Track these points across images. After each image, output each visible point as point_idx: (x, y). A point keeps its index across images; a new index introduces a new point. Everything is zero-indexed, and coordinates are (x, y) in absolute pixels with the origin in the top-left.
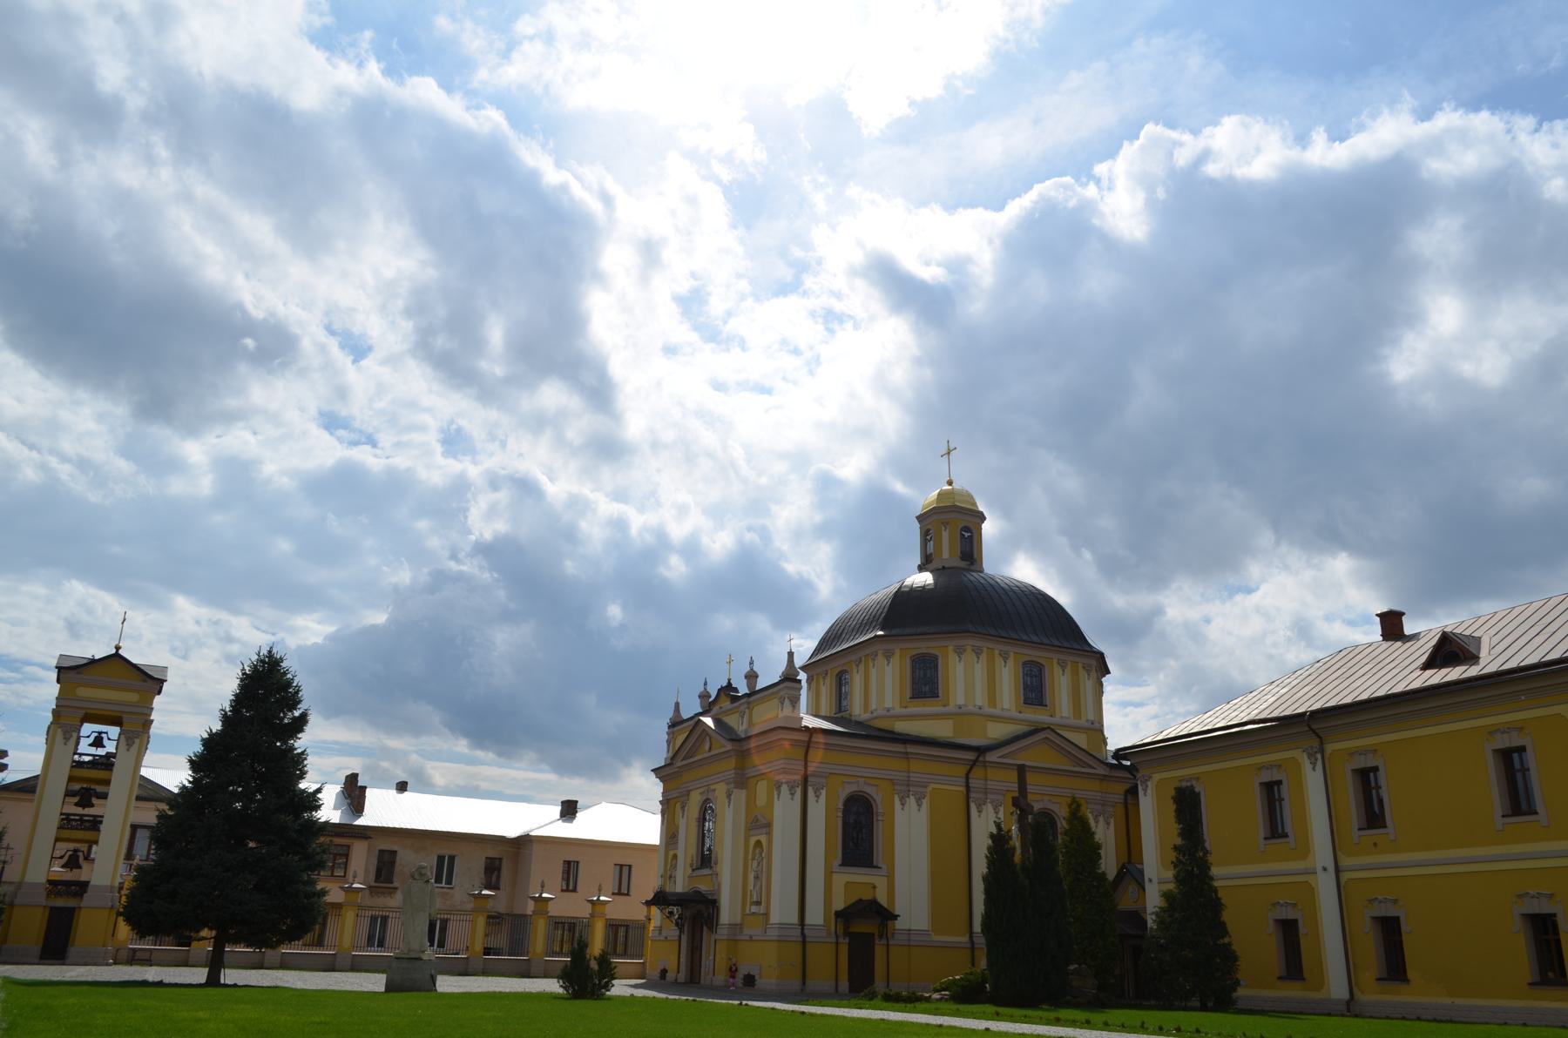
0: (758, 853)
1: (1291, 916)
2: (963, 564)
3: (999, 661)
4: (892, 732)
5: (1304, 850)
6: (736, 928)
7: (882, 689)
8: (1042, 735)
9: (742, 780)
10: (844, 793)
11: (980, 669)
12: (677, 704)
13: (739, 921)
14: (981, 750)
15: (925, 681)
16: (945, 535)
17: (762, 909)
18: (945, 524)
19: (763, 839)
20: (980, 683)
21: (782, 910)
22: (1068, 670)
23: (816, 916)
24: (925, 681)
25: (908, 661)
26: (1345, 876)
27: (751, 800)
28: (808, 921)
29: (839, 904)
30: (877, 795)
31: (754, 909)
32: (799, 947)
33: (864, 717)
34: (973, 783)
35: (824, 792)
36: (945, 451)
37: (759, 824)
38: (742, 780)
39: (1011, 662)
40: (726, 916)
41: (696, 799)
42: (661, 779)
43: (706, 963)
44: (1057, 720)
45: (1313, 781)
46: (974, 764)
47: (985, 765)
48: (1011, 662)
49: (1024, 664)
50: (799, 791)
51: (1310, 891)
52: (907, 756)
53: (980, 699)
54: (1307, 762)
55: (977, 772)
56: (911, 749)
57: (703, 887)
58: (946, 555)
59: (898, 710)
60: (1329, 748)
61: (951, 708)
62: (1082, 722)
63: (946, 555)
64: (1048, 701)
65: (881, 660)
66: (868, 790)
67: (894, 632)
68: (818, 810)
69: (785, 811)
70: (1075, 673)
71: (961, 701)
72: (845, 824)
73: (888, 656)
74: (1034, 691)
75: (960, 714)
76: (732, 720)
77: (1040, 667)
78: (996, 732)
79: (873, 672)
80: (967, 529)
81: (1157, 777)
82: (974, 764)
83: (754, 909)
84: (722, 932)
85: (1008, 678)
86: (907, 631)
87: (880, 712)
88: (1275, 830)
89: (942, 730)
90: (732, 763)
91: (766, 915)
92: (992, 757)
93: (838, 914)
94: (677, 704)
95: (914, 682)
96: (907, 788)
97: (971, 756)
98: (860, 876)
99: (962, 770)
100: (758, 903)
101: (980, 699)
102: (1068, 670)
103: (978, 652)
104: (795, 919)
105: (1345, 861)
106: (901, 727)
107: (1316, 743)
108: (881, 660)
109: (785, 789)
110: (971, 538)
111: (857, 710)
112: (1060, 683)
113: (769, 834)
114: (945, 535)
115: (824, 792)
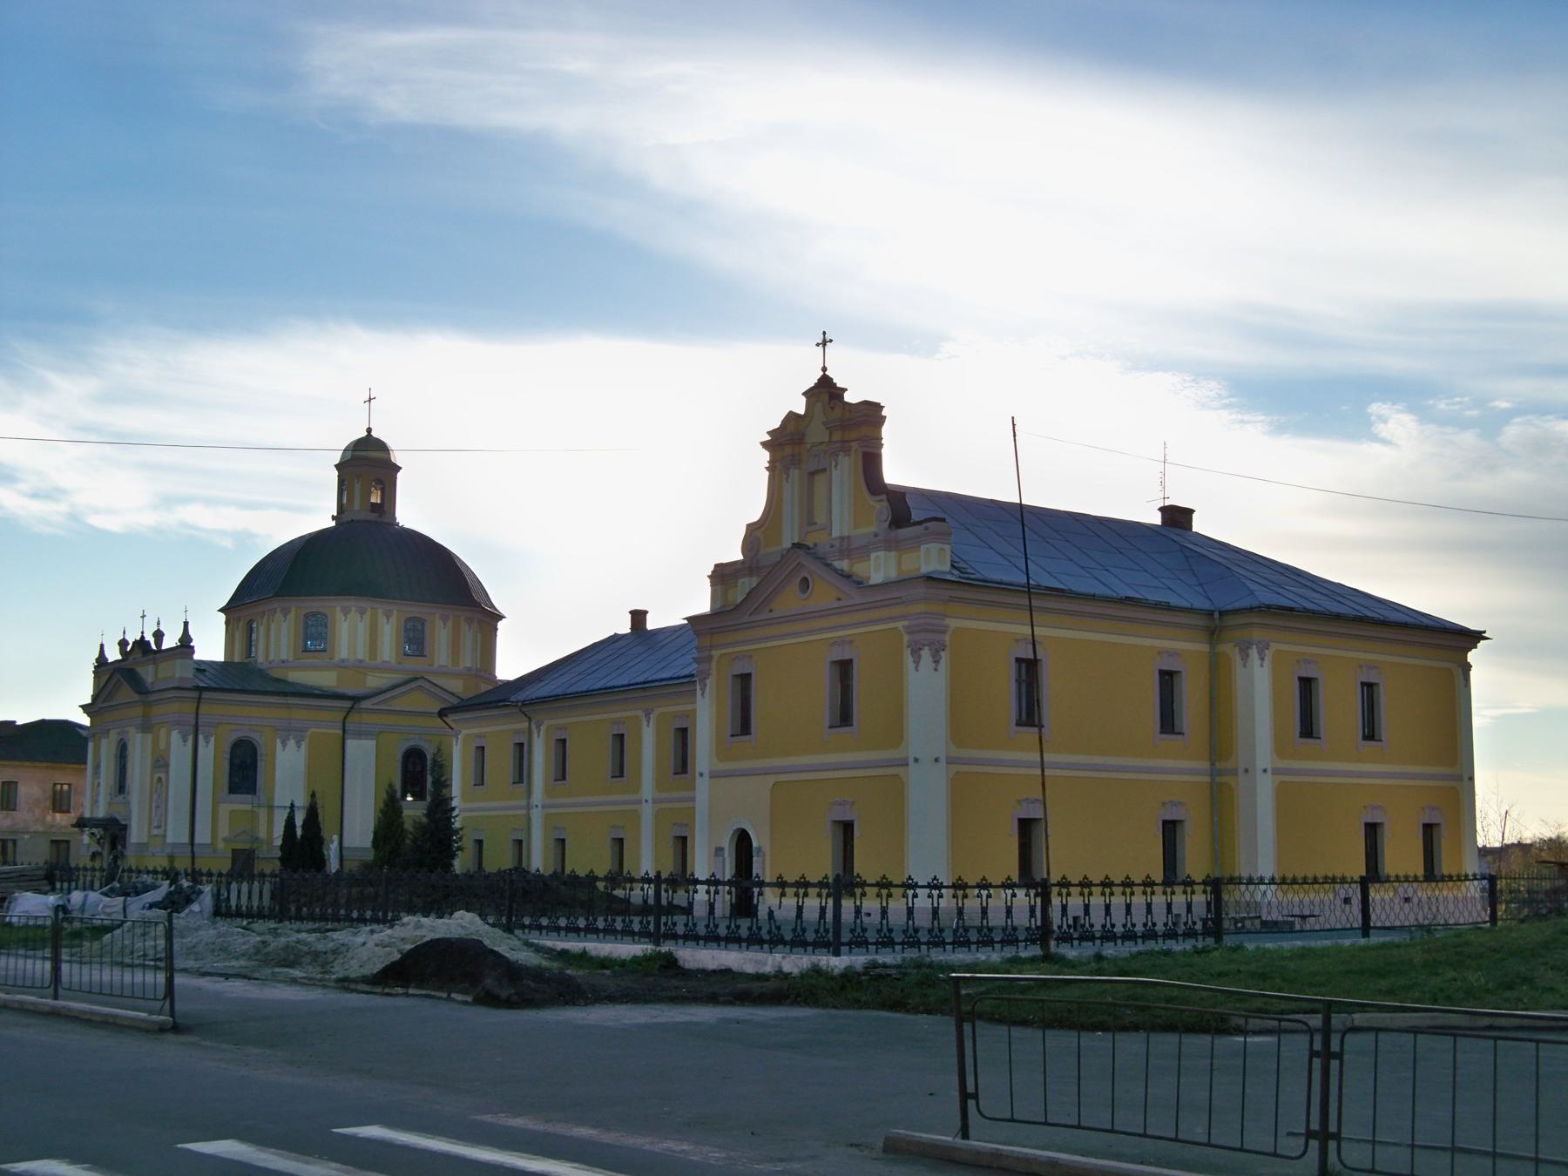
3: (382, 619)
4: (284, 681)
5: (637, 787)
8: (419, 683)
9: (146, 727)
10: (233, 737)
11: (362, 628)
12: (102, 646)
13: (145, 840)
14: (356, 699)
15: (315, 634)
19: (163, 776)
20: (362, 635)
21: (176, 833)
22: (450, 623)
27: (155, 742)
28: (197, 840)
30: (260, 739)
35: (213, 739)
37: (161, 763)
39: (393, 619)
46: (350, 710)
47: (360, 711)
48: (393, 619)
49: (408, 620)
52: (288, 706)
53: (362, 653)
54: (1238, 658)
56: (291, 700)
65: (279, 615)
66: (252, 735)
68: (207, 753)
72: (231, 760)
74: (415, 639)
75: (342, 666)
77: (423, 622)
78: (374, 681)
79: (273, 626)
81: (658, 711)
82: (350, 710)
83: (156, 832)
85: (389, 632)
88: (619, 771)
89: (326, 679)
91: (164, 836)
92: (365, 704)
94: (102, 646)
96: (287, 731)
97: (348, 704)
98: (242, 803)
99: (340, 716)
100: (158, 827)
101: (362, 653)
102: (450, 623)
104: (186, 840)
106: (296, 677)
108: (279, 615)
111: (260, 657)
112: (440, 634)
113: (167, 772)
115: (213, 739)
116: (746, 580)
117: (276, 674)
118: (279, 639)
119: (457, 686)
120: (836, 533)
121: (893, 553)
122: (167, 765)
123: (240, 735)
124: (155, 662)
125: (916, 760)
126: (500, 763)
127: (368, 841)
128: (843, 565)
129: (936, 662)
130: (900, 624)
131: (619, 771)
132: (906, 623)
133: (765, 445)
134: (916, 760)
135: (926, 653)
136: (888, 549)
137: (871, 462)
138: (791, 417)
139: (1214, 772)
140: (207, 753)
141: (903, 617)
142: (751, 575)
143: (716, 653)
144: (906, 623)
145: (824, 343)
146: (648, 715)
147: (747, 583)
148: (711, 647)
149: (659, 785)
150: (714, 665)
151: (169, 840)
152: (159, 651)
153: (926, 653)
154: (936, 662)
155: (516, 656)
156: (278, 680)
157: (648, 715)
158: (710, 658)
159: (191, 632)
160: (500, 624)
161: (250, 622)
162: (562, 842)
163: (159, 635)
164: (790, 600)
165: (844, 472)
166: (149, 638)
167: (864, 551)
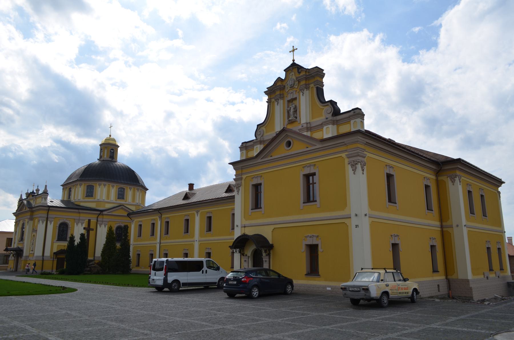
0: (34, 238)
1: (315, 243)
2: (110, 159)
4: (79, 206)
5: (193, 236)
6: (27, 257)
7: (79, 194)
9: (31, 219)
11: (105, 190)
12: (46, 186)
14: (102, 211)
15: (90, 193)
16: (106, 151)
17: (33, 252)
18: (106, 148)
20: (105, 194)
21: (38, 252)
23: (47, 253)
24: (90, 193)
25: (86, 187)
26: (161, 244)
28: (45, 255)
29: (55, 250)
31: (31, 252)
32: (41, 262)
33: (74, 201)
34: (99, 219)
36: (291, 49)
37: (35, 230)
38: (31, 219)
39: (115, 188)
40: (24, 254)
41: (21, 223)
42: (15, 216)
43: (19, 266)
44: (127, 203)
45: (197, 219)
47: (103, 215)
50: (45, 222)
51: (192, 246)
52: (79, 213)
53: (104, 198)
55: (100, 217)
56: (80, 211)
57: (20, 246)
58: (105, 157)
59: (82, 200)
60: (163, 216)
61: (96, 200)
62: (135, 203)
63: (105, 157)
64: (125, 198)
65: (79, 186)
66: (66, 221)
67: (83, 179)
68: (50, 227)
69: (41, 227)
70: (134, 191)
71: (99, 198)
72: (59, 230)
73: (81, 185)
74: (121, 195)
75: (98, 201)
76: (32, 202)
77: (124, 189)
80: (112, 150)
81: (201, 211)
82: (99, 214)
83: (31, 252)
84: (23, 258)
85: (113, 191)
86: (87, 179)
87: (77, 200)
88: (187, 231)
89: (93, 205)
90: (29, 214)
91: (34, 254)
93: (54, 253)
94: (46, 186)
95: (87, 192)
96: (78, 221)
97: (99, 212)
101: (104, 198)
102: (132, 190)
103: (105, 185)
104: (41, 254)
105: (162, 241)
107: (160, 215)
108: (79, 186)
109: (41, 222)
110: (113, 152)
111: (72, 199)
112: (129, 193)
114: (106, 151)
116: (258, 146)
117: (76, 203)
118: (79, 194)
119: (133, 208)
120: (303, 121)
121: (335, 126)
122: (36, 231)
123: (61, 221)
124: (36, 199)
125: (356, 215)
126: (147, 230)
127: (100, 255)
128: (308, 134)
129: (363, 170)
130: (344, 155)
131: (187, 231)
132: (347, 153)
133: (266, 93)
134: (356, 215)
135: (359, 166)
136: (333, 124)
137: (320, 92)
138: (279, 79)
139: (442, 227)
140: (50, 227)
141: (346, 151)
142: (260, 144)
143: (244, 177)
144: (347, 153)
145: (293, 51)
146: (197, 213)
147: (258, 148)
148: (242, 174)
149: (201, 235)
150: (243, 181)
151: (35, 255)
152: (38, 195)
153: (359, 166)
154: (363, 170)
155: (152, 199)
156: (77, 205)
157: (197, 213)
158: (241, 179)
159: (48, 189)
160: (147, 192)
161: (70, 188)
162: (139, 255)
163: (38, 190)
164: (282, 150)
165: (305, 101)
166: (35, 191)
167: (321, 126)
